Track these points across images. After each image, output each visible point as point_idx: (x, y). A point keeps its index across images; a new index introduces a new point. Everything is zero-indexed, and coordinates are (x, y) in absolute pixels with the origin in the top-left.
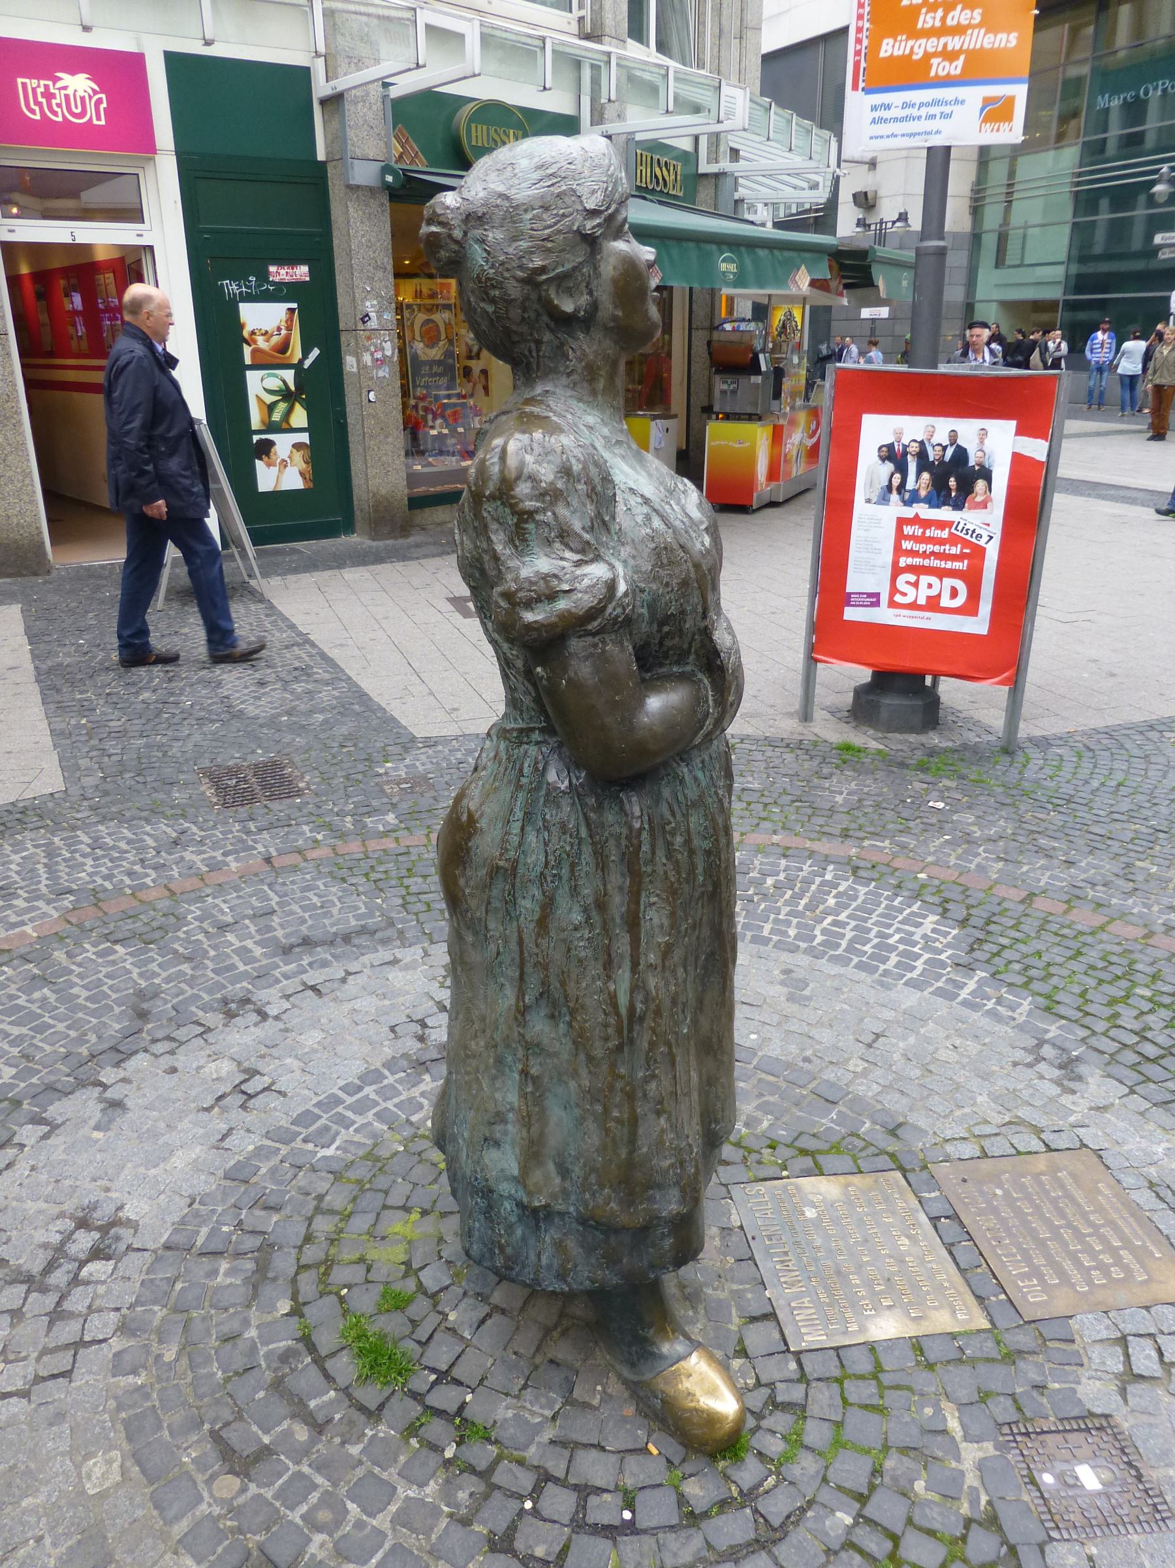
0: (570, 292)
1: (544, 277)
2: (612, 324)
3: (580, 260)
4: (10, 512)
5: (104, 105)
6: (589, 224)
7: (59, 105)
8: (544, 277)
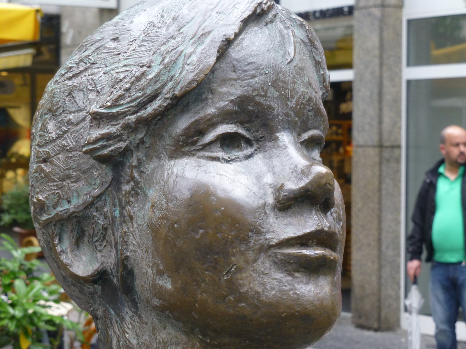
6: (96, 133)
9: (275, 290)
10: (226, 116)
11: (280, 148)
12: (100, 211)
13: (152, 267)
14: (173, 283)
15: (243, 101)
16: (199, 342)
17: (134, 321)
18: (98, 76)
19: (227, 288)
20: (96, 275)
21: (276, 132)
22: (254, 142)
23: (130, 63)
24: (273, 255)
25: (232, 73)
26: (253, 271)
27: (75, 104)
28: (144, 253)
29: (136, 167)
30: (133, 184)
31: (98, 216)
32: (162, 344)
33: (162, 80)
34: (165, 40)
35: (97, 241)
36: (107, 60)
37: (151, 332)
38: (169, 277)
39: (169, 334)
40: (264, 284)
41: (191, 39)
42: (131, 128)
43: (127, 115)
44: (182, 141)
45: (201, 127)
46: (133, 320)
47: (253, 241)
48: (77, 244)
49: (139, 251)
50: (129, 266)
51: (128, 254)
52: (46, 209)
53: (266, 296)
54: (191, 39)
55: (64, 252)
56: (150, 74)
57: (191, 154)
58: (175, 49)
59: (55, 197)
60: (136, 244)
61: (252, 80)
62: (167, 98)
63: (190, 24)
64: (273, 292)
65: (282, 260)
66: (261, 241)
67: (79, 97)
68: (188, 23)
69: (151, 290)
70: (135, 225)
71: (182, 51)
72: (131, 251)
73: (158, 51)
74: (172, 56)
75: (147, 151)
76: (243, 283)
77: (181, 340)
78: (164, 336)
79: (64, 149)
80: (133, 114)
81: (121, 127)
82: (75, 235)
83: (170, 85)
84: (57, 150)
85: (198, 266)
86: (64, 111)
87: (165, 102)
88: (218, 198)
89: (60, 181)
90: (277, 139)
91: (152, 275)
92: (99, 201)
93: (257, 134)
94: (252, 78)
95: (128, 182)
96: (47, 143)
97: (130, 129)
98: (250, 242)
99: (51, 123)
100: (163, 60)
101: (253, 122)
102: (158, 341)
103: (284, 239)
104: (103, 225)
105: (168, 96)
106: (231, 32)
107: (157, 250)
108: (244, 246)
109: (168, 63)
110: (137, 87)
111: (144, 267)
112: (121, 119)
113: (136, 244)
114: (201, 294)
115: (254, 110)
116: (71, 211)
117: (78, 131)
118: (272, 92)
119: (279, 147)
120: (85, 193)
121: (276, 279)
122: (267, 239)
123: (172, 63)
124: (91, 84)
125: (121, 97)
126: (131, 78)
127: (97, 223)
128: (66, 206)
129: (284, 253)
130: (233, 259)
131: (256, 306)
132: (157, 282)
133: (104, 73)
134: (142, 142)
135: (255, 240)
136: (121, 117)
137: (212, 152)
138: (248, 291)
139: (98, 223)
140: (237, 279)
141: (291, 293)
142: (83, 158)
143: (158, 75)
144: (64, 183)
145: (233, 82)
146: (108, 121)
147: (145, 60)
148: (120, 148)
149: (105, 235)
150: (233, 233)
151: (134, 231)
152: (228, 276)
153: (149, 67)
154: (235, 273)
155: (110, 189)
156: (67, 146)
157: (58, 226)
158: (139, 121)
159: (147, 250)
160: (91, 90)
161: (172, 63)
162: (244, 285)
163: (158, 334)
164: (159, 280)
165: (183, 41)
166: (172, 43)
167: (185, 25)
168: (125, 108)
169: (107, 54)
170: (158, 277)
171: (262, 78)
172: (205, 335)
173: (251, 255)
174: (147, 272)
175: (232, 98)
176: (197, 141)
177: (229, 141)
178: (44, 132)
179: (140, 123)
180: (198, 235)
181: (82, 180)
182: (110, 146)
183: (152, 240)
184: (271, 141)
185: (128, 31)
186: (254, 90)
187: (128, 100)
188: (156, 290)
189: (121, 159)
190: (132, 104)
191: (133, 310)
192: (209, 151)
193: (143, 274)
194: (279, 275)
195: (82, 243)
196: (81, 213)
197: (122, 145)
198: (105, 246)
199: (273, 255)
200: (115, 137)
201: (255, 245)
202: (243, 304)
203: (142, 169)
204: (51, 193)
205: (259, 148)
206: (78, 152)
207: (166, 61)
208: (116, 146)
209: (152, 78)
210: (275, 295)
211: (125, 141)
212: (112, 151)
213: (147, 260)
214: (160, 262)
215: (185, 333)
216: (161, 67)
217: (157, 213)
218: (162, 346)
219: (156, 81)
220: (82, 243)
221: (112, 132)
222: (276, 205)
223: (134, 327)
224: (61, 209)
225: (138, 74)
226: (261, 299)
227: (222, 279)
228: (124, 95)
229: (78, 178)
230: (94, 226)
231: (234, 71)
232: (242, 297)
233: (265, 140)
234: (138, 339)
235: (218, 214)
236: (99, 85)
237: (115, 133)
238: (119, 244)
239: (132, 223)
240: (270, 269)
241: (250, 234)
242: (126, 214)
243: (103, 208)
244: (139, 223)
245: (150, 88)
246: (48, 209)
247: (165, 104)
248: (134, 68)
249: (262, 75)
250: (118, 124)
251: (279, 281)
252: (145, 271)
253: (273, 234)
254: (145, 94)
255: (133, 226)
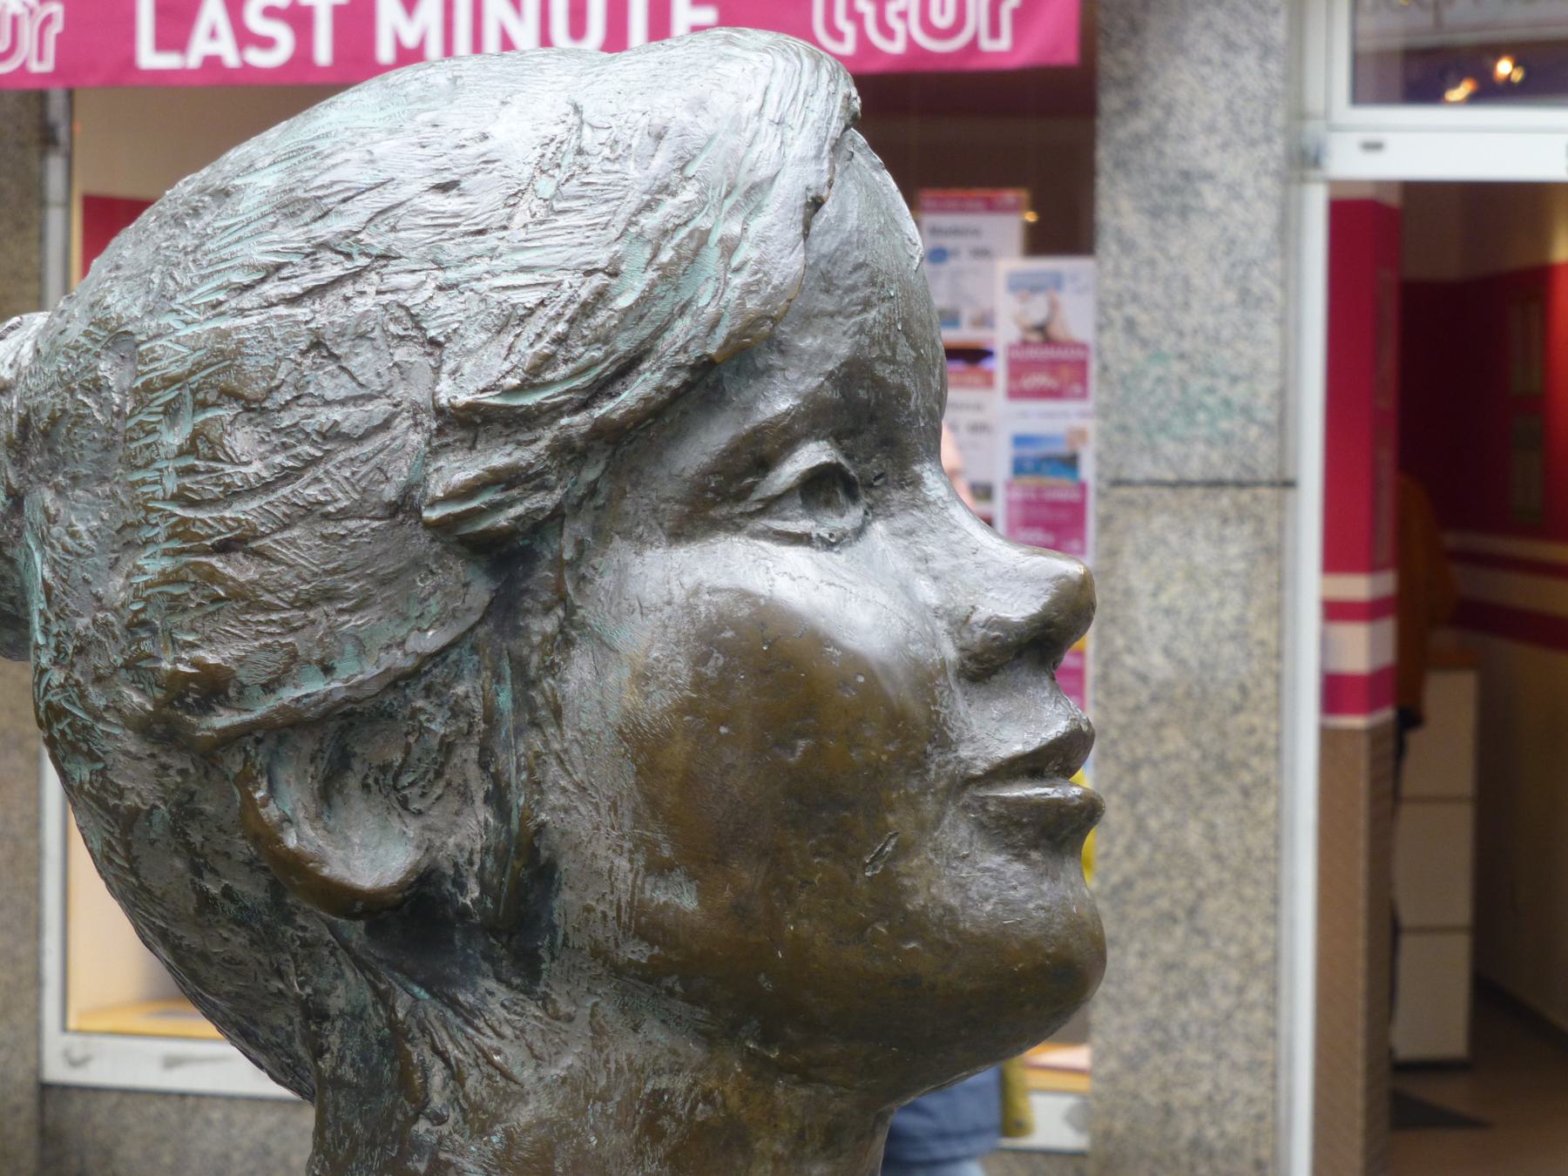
0: (393, 792)
1: (223, 719)
2: (636, 952)
3: (432, 640)
4: (1179, 1096)
5: (57, 27)
6: (459, 469)
7: (903, 15)
8: (223, 719)
9: (992, 901)
10: (814, 419)
11: (932, 507)
12: (439, 694)
13: (630, 851)
14: (703, 894)
15: (853, 373)
16: (742, 1061)
17: (521, 1015)
18: (421, 296)
19: (873, 901)
20: (411, 886)
21: (914, 462)
22: (860, 491)
23: (540, 262)
24: (976, 805)
25: (822, 296)
26: (934, 850)
27: (345, 378)
28: (603, 811)
29: (571, 564)
30: (561, 613)
31: (430, 708)
32: (628, 1075)
33: (657, 313)
34: (647, 197)
35: (412, 784)
36: (441, 248)
37: (589, 1043)
38: (691, 877)
39: (650, 1043)
40: (961, 886)
41: (726, 196)
42: (572, 450)
43: (561, 415)
44: (713, 490)
45: (767, 448)
46: (515, 1013)
47: (933, 767)
48: (327, 794)
49: (582, 809)
50: (545, 854)
51: (543, 817)
52: (232, 693)
53: (974, 919)
54: (726, 196)
55: (290, 821)
56: (620, 294)
57: (733, 526)
58: (685, 224)
59: (276, 657)
60: (571, 788)
61: (865, 315)
62: (679, 367)
63: (709, 152)
64: (988, 907)
65: (1000, 817)
66: (950, 767)
67: (364, 361)
68: (702, 149)
69: (625, 918)
70: (569, 734)
71: (709, 231)
72: (553, 809)
73: (633, 230)
74: (679, 246)
75: (597, 518)
76: (914, 885)
77: (688, 1057)
78: (635, 1051)
79: (311, 512)
80: (576, 411)
81: (547, 448)
82: (321, 768)
83: (682, 327)
84: (285, 515)
85: (793, 843)
86: (298, 397)
87: (671, 377)
88: (845, 650)
89: (294, 607)
90: (917, 482)
91: (631, 876)
92: (435, 666)
93: (868, 466)
94: (864, 310)
95: (548, 610)
96: (235, 493)
97: (568, 453)
98: (928, 771)
99: (239, 434)
100: (655, 256)
101: (861, 433)
102: (613, 1066)
103: (1004, 760)
104: (445, 736)
105: (682, 358)
106: (813, 176)
107: (653, 802)
108: (915, 782)
109: (671, 262)
110: (586, 332)
111: (601, 852)
112: (542, 426)
113: (571, 788)
114: (794, 923)
115: (869, 400)
116: (339, 696)
117: (368, 460)
118: (905, 353)
119: (928, 503)
120: (385, 641)
121: (988, 869)
122: (960, 761)
123: (684, 264)
124: (396, 320)
125: (547, 361)
126: (565, 306)
127: (422, 731)
128: (315, 686)
129: (1005, 798)
130: (891, 819)
131: (947, 947)
132: (648, 894)
133: (440, 288)
134: (593, 490)
135: (939, 766)
136: (544, 420)
137: (785, 519)
138: (925, 906)
139: (429, 730)
140: (899, 874)
141: (1031, 906)
142: (385, 540)
143: (645, 299)
144: (312, 615)
145: (826, 321)
146: (506, 432)
147: (602, 258)
148: (542, 509)
149: (442, 765)
150: (891, 748)
151: (566, 751)
152: (875, 868)
153: (614, 275)
154: (894, 857)
155: (481, 631)
156: (326, 503)
157: (270, 743)
158: (606, 433)
159: (614, 803)
160: (402, 338)
161: (684, 264)
162: (915, 891)
163: (611, 1047)
164: (655, 887)
165: (705, 203)
166: (669, 206)
167: (694, 156)
168: (560, 394)
169: (431, 230)
170: (651, 880)
171: (885, 307)
172: (766, 1040)
173: (929, 806)
174: (611, 870)
175: (830, 367)
176: (751, 489)
177: (820, 488)
178: (216, 459)
179: (598, 438)
180: (793, 754)
181: (375, 603)
182: (510, 504)
183: (638, 773)
184: (902, 487)
185: (486, 162)
186: (874, 342)
187: (563, 370)
188: (643, 919)
189: (527, 542)
190: (577, 383)
191: (516, 981)
192: (778, 518)
193: (599, 873)
194: (995, 860)
195: (340, 792)
196: (368, 704)
197: (545, 501)
198: (439, 798)
199: (976, 805)
200: (529, 479)
201: (939, 777)
202: (913, 945)
203: (583, 570)
204: (257, 644)
205: (871, 507)
206: (365, 522)
207: (665, 256)
208: (527, 504)
209: (630, 308)
210: (993, 916)
211: (551, 489)
212: (518, 518)
213: (614, 833)
214: (660, 837)
215: (708, 1038)
216: (651, 275)
217: (656, 696)
218: (627, 1082)
219: (642, 317)
220: (340, 792)
221: (523, 464)
222: (963, 665)
223: (523, 1031)
224: (298, 693)
225: (584, 293)
226: (961, 926)
227: (859, 875)
228: (553, 356)
229: (365, 599)
230: (411, 739)
231: (827, 291)
232: (913, 925)
233: (886, 483)
234: (539, 1065)
235: (849, 695)
236: (434, 323)
237: (531, 465)
238: (514, 788)
239: (559, 726)
240: (971, 844)
241: (929, 748)
242: (539, 700)
243: (448, 686)
244: (583, 726)
245: (625, 335)
246: (240, 693)
247: (675, 383)
248: (568, 279)
249: (883, 300)
250: (535, 441)
251: (997, 874)
252: (603, 865)
253: (972, 746)
254: (613, 353)
255: (562, 735)
